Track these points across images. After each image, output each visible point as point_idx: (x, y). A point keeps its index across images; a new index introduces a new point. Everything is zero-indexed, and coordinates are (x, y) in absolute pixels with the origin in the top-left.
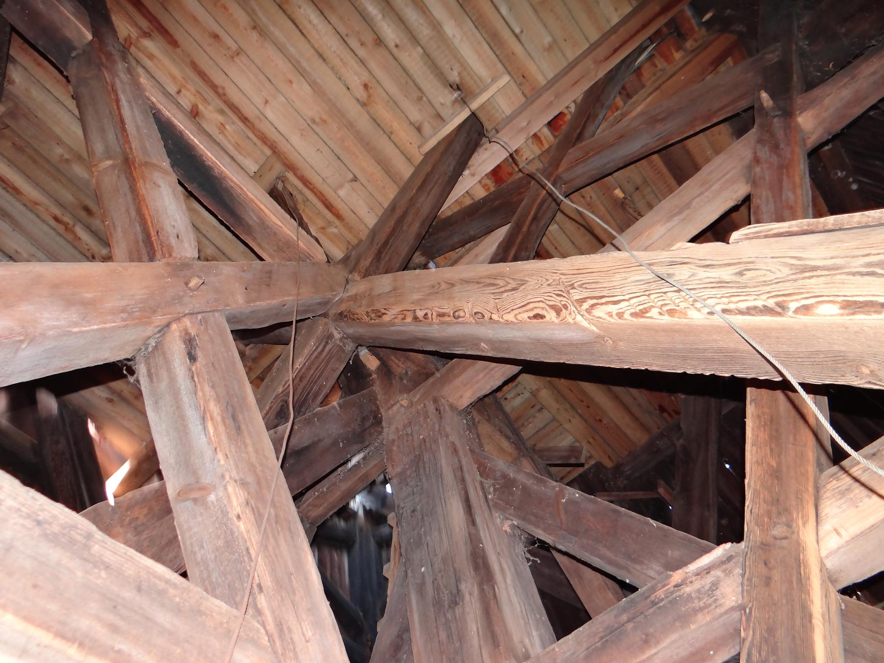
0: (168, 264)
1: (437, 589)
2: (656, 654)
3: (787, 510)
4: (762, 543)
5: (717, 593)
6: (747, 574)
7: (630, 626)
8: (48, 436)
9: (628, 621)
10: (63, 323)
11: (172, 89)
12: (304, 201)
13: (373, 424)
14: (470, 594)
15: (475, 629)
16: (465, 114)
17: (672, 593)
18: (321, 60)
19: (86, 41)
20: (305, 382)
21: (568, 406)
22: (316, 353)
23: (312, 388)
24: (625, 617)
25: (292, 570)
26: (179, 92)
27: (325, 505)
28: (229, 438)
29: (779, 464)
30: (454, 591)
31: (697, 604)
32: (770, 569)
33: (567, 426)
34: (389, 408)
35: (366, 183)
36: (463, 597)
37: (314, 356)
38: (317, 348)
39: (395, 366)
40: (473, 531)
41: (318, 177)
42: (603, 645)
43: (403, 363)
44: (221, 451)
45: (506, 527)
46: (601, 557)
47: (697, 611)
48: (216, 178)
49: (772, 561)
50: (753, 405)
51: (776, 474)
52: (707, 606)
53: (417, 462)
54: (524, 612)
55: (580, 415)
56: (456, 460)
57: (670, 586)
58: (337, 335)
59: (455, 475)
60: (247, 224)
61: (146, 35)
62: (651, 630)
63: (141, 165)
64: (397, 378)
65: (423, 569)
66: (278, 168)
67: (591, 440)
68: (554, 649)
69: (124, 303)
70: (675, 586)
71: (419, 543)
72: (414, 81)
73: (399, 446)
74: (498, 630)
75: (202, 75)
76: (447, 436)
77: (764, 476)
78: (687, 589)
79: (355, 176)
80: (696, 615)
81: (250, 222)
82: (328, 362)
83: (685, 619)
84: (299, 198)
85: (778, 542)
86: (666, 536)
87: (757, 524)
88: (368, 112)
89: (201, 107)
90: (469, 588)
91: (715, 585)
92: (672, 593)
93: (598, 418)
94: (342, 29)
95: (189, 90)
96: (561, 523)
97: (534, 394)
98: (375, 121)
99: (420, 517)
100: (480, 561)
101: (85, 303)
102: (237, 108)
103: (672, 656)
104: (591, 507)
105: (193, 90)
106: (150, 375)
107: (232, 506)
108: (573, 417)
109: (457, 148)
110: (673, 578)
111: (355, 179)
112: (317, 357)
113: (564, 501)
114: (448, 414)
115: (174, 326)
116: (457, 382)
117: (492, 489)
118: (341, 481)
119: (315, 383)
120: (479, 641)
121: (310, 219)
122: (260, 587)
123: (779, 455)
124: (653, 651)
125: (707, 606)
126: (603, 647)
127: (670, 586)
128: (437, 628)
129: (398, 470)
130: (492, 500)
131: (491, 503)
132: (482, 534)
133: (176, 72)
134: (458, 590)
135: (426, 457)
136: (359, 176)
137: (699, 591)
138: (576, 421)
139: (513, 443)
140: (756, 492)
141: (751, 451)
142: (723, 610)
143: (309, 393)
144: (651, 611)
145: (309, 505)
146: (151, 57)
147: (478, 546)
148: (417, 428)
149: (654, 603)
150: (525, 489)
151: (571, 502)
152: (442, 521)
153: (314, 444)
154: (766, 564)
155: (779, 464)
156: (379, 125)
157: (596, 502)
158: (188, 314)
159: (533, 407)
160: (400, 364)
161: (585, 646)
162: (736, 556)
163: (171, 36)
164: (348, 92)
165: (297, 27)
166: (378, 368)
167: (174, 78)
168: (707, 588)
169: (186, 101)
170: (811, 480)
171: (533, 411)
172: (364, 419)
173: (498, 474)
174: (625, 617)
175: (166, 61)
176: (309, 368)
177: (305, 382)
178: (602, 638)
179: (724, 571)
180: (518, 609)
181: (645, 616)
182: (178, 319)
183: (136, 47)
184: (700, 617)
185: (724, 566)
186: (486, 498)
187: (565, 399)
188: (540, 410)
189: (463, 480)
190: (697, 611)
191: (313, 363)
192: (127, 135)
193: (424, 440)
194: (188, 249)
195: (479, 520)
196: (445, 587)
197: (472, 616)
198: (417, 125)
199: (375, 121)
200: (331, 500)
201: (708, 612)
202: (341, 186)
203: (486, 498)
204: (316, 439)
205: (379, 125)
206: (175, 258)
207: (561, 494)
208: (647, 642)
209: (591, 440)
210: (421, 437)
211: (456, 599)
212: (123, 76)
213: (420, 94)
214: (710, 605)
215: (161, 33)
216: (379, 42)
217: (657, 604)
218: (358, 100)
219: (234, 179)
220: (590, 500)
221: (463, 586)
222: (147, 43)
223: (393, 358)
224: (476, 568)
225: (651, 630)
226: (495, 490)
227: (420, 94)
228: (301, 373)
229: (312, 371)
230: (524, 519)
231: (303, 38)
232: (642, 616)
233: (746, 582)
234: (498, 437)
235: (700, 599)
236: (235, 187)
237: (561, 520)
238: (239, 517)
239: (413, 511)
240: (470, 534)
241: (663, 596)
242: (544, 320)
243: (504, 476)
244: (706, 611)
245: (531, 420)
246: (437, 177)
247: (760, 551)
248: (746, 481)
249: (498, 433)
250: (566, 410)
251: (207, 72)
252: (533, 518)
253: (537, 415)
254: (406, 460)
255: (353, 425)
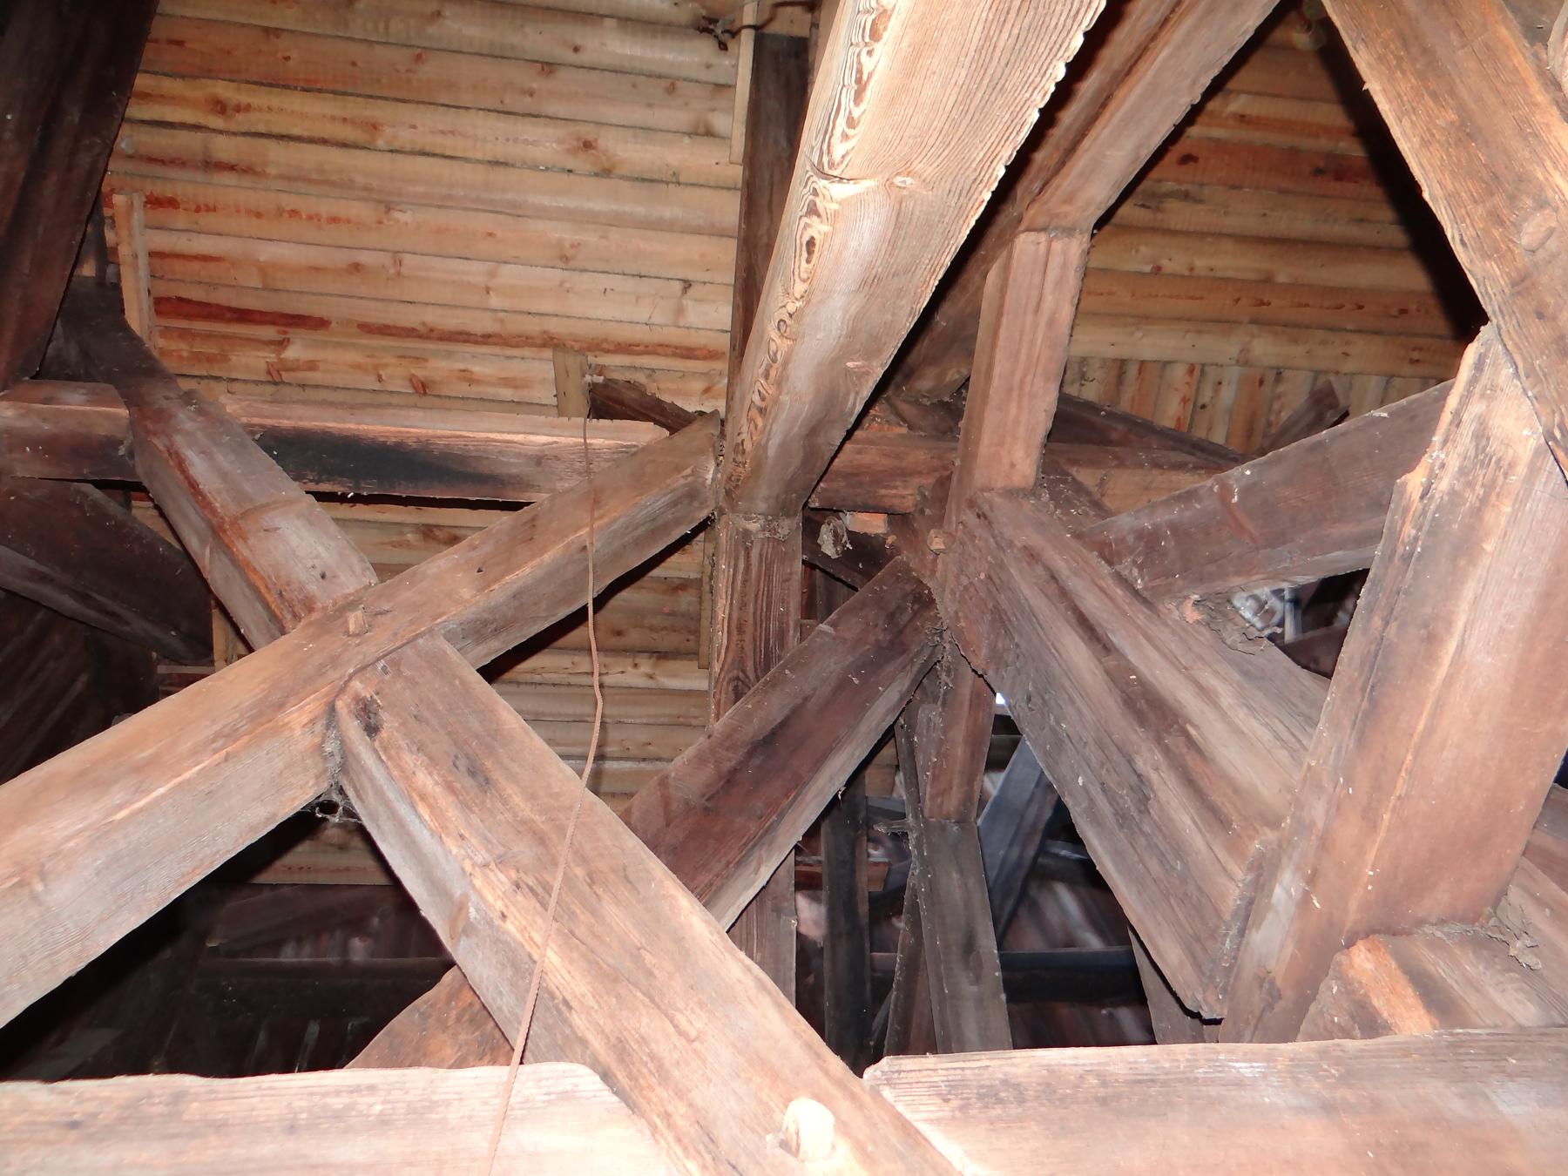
0: (310, 624)
1: (1112, 799)
2: (1462, 646)
3: (1523, 179)
4: (1514, 284)
5: (1494, 446)
6: (1520, 365)
7: (1393, 628)
8: (283, 965)
9: (1386, 624)
10: (95, 817)
11: (370, 382)
12: (649, 376)
13: (915, 614)
14: (1156, 769)
15: (1188, 822)
16: (745, 47)
17: (1424, 512)
18: (501, 170)
19: (125, 422)
20: (749, 629)
21: (1320, 334)
22: (740, 577)
23: (767, 633)
24: (1377, 622)
25: (635, 937)
26: (380, 379)
27: (956, 781)
28: (466, 806)
29: (1461, 109)
30: (1134, 780)
31: (1471, 498)
32: (1554, 319)
33: (1349, 366)
34: (933, 572)
35: (707, 277)
36: (1149, 781)
37: (739, 584)
38: (736, 566)
39: (896, 501)
40: (1111, 662)
41: (638, 327)
42: (1371, 699)
43: (905, 488)
44: (448, 835)
45: (1192, 615)
46: (1340, 545)
47: (1479, 509)
48: (415, 452)
49: (1550, 300)
50: (1361, 47)
51: (1467, 132)
52: (1490, 487)
53: (1000, 619)
54: (1285, 735)
55: (1359, 331)
56: (1040, 570)
57: (1416, 505)
58: (754, 526)
59: (1046, 595)
60: (510, 476)
61: (282, 344)
62: (1428, 610)
63: (234, 523)
64: (917, 515)
65: (1080, 781)
66: (572, 362)
67: (1415, 355)
68: (1309, 767)
69: (216, 728)
70: (1422, 498)
71: (1058, 744)
72: (641, 73)
73: (966, 617)
74: (1216, 798)
75: (385, 331)
76: (1011, 544)
77: (1449, 156)
78: (1443, 485)
79: (685, 281)
80: (1482, 519)
81: (514, 471)
82: (769, 576)
83: (1466, 548)
84: (640, 378)
85: (1541, 254)
86: (1412, 418)
87: (1486, 256)
88: (622, 177)
89: (420, 373)
90: (1149, 760)
91: (1481, 436)
92: (1424, 512)
93: (1394, 311)
94: (490, 102)
95: (387, 365)
96: (1253, 540)
97: (1244, 361)
98: (643, 180)
99: (1040, 702)
100: (1142, 705)
101: (139, 769)
102: (460, 333)
103: (1502, 630)
104: (1276, 474)
105: (394, 360)
106: (359, 797)
107: (490, 906)
108: (1348, 343)
109: (773, 105)
110: (1409, 488)
111: (687, 285)
112: (745, 582)
113: (1236, 499)
114: (1002, 510)
115: (339, 704)
116: (984, 449)
117: (1135, 572)
118: (945, 730)
119: (768, 619)
120: (1204, 836)
121: (678, 393)
122: (566, 1003)
123: (1452, 92)
124: (1452, 646)
125: (1490, 487)
126: (1374, 703)
127: (1416, 505)
128: (1142, 861)
129: (984, 651)
130: (1145, 588)
131: (1146, 594)
132: (1133, 657)
133: (352, 357)
134: (1139, 776)
135: (1004, 605)
136: (690, 276)
137: (1463, 472)
138: (1360, 345)
139: (1196, 468)
140: (1452, 198)
141: (1404, 133)
142: (1522, 469)
143: (767, 641)
144: (1410, 574)
145: (933, 797)
146: (312, 366)
147: (1128, 683)
148: (972, 568)
149: (1407, 558)
150: (1175, 528)
151: (1248, 490)
152: (1067, 684)
153: (796, 712)
154: (1540, 316)
155: (1461, 109)
156: (652, 181)
157: (1279, 460)
158: (355, 673)
159: (1261, 382)
160: (901, 491)
161: (1347, 723)
162: (1488, 351)
163: (310, 318)
164: (572, 176)
165: (434, 155)
166: (890, 523)
167: (358, 367)
168: (1472, 453)
169: (397, 377)
170: (1530, 74)
171: (1267, 389)
172: (891, 617)
173: (1131, 539)
174: (1377, 622)
175: (330, 355)
176: (743, 606)
177: (749, 629)
178: (1363, 689)
179: (1483, 396)
180: (1266, 736)
181: (1407, 593)
182: (342, 690)
183: (287, 370)
184: (1489, 516)
185: (1478, 390)
186: (1136, 593)
187: (1307, 327)
188: (1279, 377)
189: (1064, 593)
190: (1479, 509)
191: (744, 594)
192: (204, 497)
193: (989, 577)
194: (354, 577)
195: (1117, 639)
196: (1119, 784)
197: (1174, 803)
198: (702, 130)
199: (643, 180)
200: (958, 768)
201: (1498, 495)
202: (680, 311)
203: (1136, 593)
204: (799, 701)
205: (652, 181)
206: (324, 608)
207: (1226, 490)
208: (1432, 639)
209: (1415, 355)
210: (982, 576)
211: (1142, 793)
212: (188, 426)
213: (664, 83)
214: (1494, 481)
215: (298, 325)
216: (548, 67)
217: (1412, 554)
218: (596, 175)
219: (439, 432)
220: (1269, 463)
221: (1140, 765)
222: (293, 353)
223: (883, 492)
224: (1141, 719)
225: (1428, 610)
226: (1141, 568)
227: (664, 83)
228: (735, 621)
229: (751, 608)
230: (1201, 580)
231: (454, 163)
232: (1402, 596)
233: (1527, 384)
234: (1160, 478)
235: (1470, 485)
236: (452, 441)
237: (1251, 534)
238: (504, 916)
239: (1029, 700)
240: (1107, 672)
241: (1413, 532)
242: (817, 243)
243: (1140, 535)
244: (1493, 498)
245: (1276, 406)
246: (767, 176)
247: (1520, 301)
248: (1426, 196)
249: (1155, 472)
250: (1324, 343)
251: (390, 323)
252: (1212, 568)
253: (1281, 389)
254: (984, 629)
255: (872, 638)
